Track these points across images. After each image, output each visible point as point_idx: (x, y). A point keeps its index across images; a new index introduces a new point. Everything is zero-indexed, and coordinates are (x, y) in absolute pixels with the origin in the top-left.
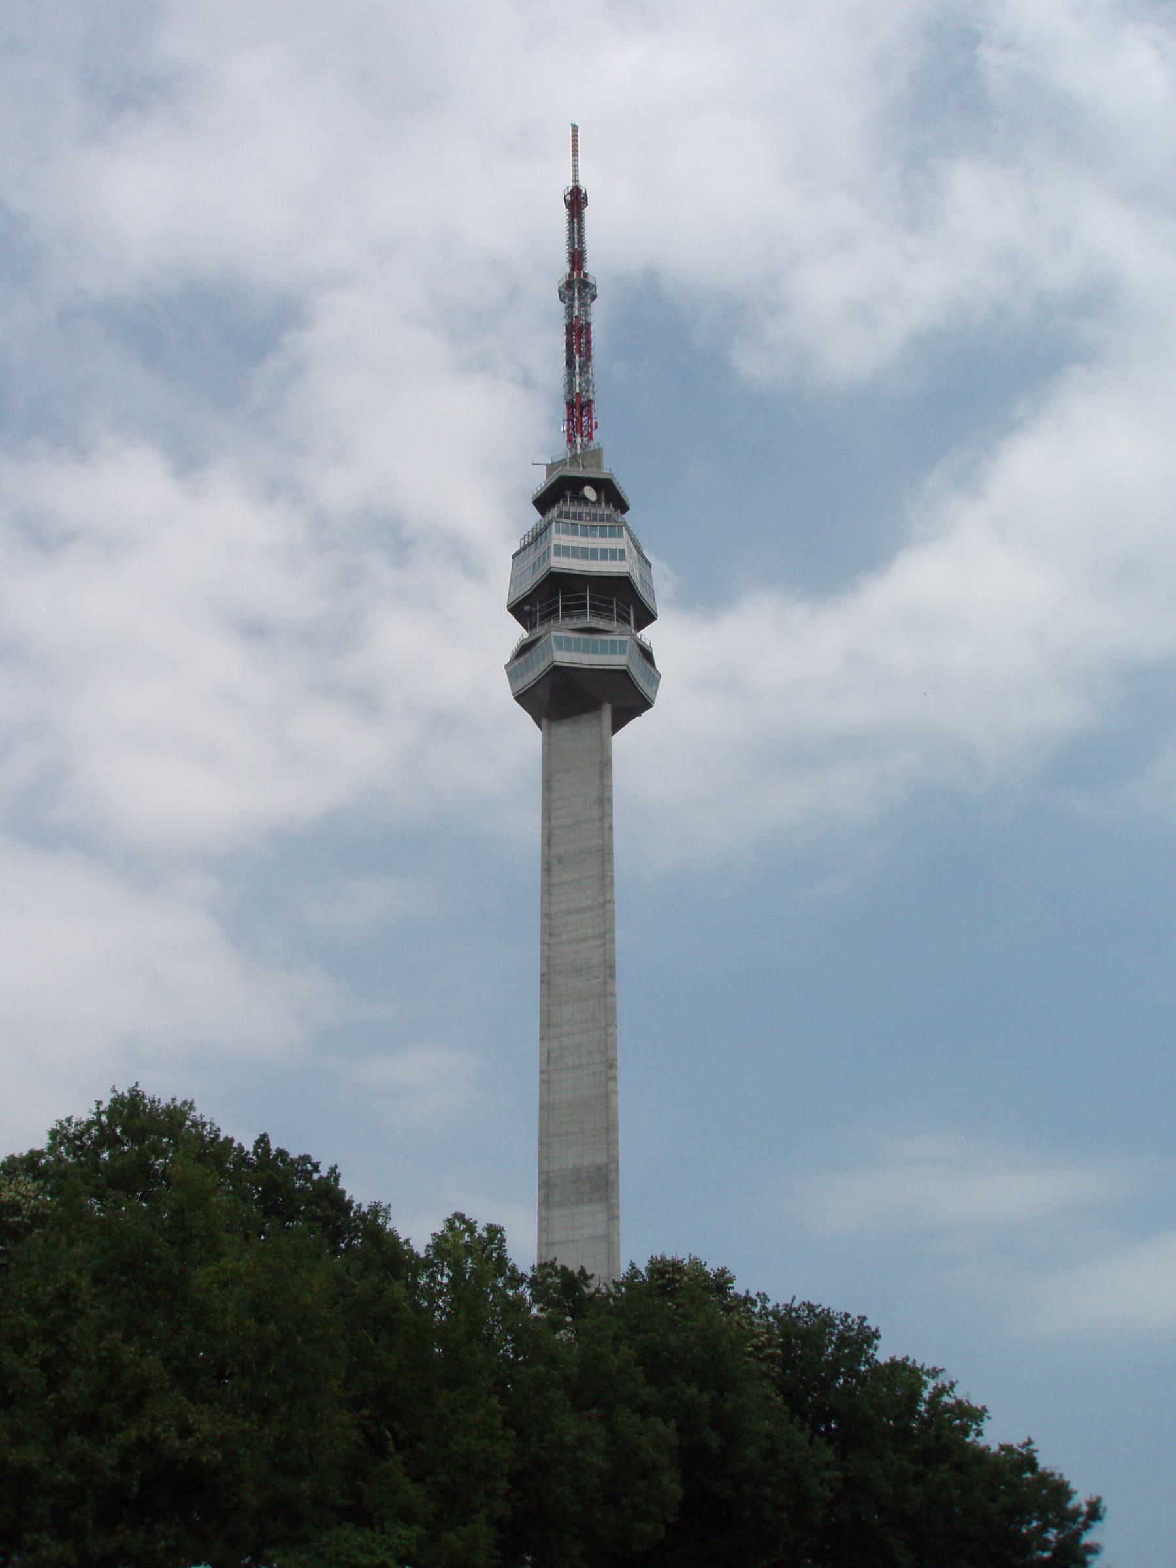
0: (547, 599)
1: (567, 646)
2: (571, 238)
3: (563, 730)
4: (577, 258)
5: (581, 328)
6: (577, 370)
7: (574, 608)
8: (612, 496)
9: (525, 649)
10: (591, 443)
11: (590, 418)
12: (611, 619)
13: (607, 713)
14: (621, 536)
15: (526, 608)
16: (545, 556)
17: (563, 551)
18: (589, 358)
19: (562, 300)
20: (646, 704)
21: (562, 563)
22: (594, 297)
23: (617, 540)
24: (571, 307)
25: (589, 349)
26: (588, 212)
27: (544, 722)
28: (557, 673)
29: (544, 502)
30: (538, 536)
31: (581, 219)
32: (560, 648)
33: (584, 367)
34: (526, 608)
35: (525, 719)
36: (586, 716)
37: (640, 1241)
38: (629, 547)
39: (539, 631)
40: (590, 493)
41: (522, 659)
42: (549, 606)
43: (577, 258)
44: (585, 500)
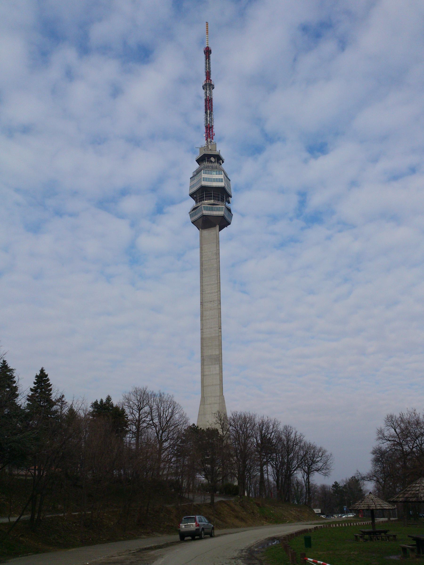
0: (201, 194)
1: (207, 209)
2: (206, 67)
3: (206, 232)
4: (208, 74)
5: (210, 128)
6: (208, 116)
7: (209, 197)
8: (219, 158)
9: (194, 209)
10: (213, 141)
11: (212, 132)
12: (219, 200)
13: (218, 227)
14: (222, 174)
15: (195, 196)
16: (200, 181)
17: (205, 179)
18: (212, 111)
19: (204, 89)
20: (229, 224)
21: (204, 183)
22: (213, 88)
23: (220, 176)
24: (206, 93)
25: (212, 107)
26: (211, 55)
27: (200, 229)
28: (204, 217)
29: (199, 161)
30: (198, 172)
31: (209, 59)
32: (205, 210)
33: (211, 114)
34: (195, 196)
35: (194, 228)
36: (212, 228)
37: (240, 401)
38: (224, 177)
39: (199, 204)
40: (213, 159)
41: (194, 211)
42: (201, 195)
43: (208, 74)
44: (211, 162)
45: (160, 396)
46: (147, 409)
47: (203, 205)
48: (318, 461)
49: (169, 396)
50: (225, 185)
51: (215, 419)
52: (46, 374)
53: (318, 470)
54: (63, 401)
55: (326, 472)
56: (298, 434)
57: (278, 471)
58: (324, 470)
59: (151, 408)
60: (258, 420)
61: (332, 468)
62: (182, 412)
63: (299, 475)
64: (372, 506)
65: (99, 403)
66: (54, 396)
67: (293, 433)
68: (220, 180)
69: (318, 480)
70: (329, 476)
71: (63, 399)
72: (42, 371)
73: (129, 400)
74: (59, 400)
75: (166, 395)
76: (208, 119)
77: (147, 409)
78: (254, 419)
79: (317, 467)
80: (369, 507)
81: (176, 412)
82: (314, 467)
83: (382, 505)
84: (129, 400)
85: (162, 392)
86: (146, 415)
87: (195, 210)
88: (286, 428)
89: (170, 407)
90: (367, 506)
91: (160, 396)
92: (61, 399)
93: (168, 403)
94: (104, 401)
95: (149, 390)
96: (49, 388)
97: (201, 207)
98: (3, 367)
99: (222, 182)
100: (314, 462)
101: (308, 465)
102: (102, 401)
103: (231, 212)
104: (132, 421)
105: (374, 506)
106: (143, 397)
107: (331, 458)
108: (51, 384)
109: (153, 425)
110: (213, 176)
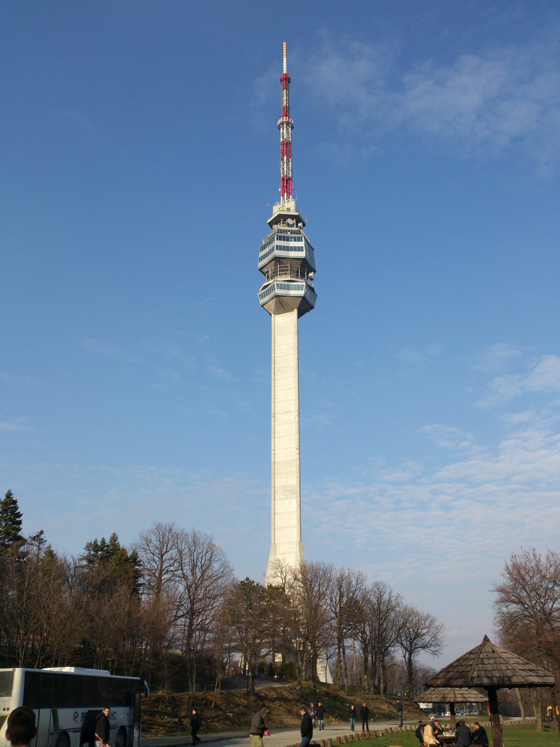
1: (281, 287)
7: (284, 272)
20: (312, 308)
23: (300, 242)
32: (278, 288)
38: (305, 245)
45: (195, 536)
46: (173, 553)
47: (275, 282)
48: (424, 634)
49: (206, 536)
50: (306, 255)
51: (274, 571)
52: (14, 499)
53: (424, 647)
54: (42, 539)
55: (437, 649)
56: (394, 594)
57: (366, 646)
58: (432, 646)
59: (180, 553)
60: (335, 574)
61: (444, 643)
62: (224, 560)
63: (398, 654)
64: (450, 696)
65: (99, 544)
66: (27, 530)
67: (387, 593)
68: (299, 249)
69: (429, 661)
70: (440, 655)
71: (42, 536)
72: (9, 495)
73: (148, 541)
74: (35, 537)
75: (202, 535)
76: (285, 169)
77: (173, 553)
78: (330, 572)
79: (422, 642)
80: (444, 698)
81: (216, 559)
82: (419, 642)
83: (465, 696)
84: (148, 541)
85: (196, 530)
86: (172, 562)
87: (267, 289)
88: (377, 585)
89: (207, 552)
90: (442, 696)
91: (195, 536)
92: (38, 538)
93: (206, 546)
94: (107, 541)
95: (177, 528)
96: (18, 519)
97: (274, 285)
98: (5, 504)
99: (302, 251)
100: (418, 635)
101: (411, 639)
102: (103, 541)
103: (314, 292)
104: (149, 570)
105: (453, 696)
106: (166, 538)
107: (442, 629)
108: (21, 513)
109: (184, 578)
110: (290, 243)
